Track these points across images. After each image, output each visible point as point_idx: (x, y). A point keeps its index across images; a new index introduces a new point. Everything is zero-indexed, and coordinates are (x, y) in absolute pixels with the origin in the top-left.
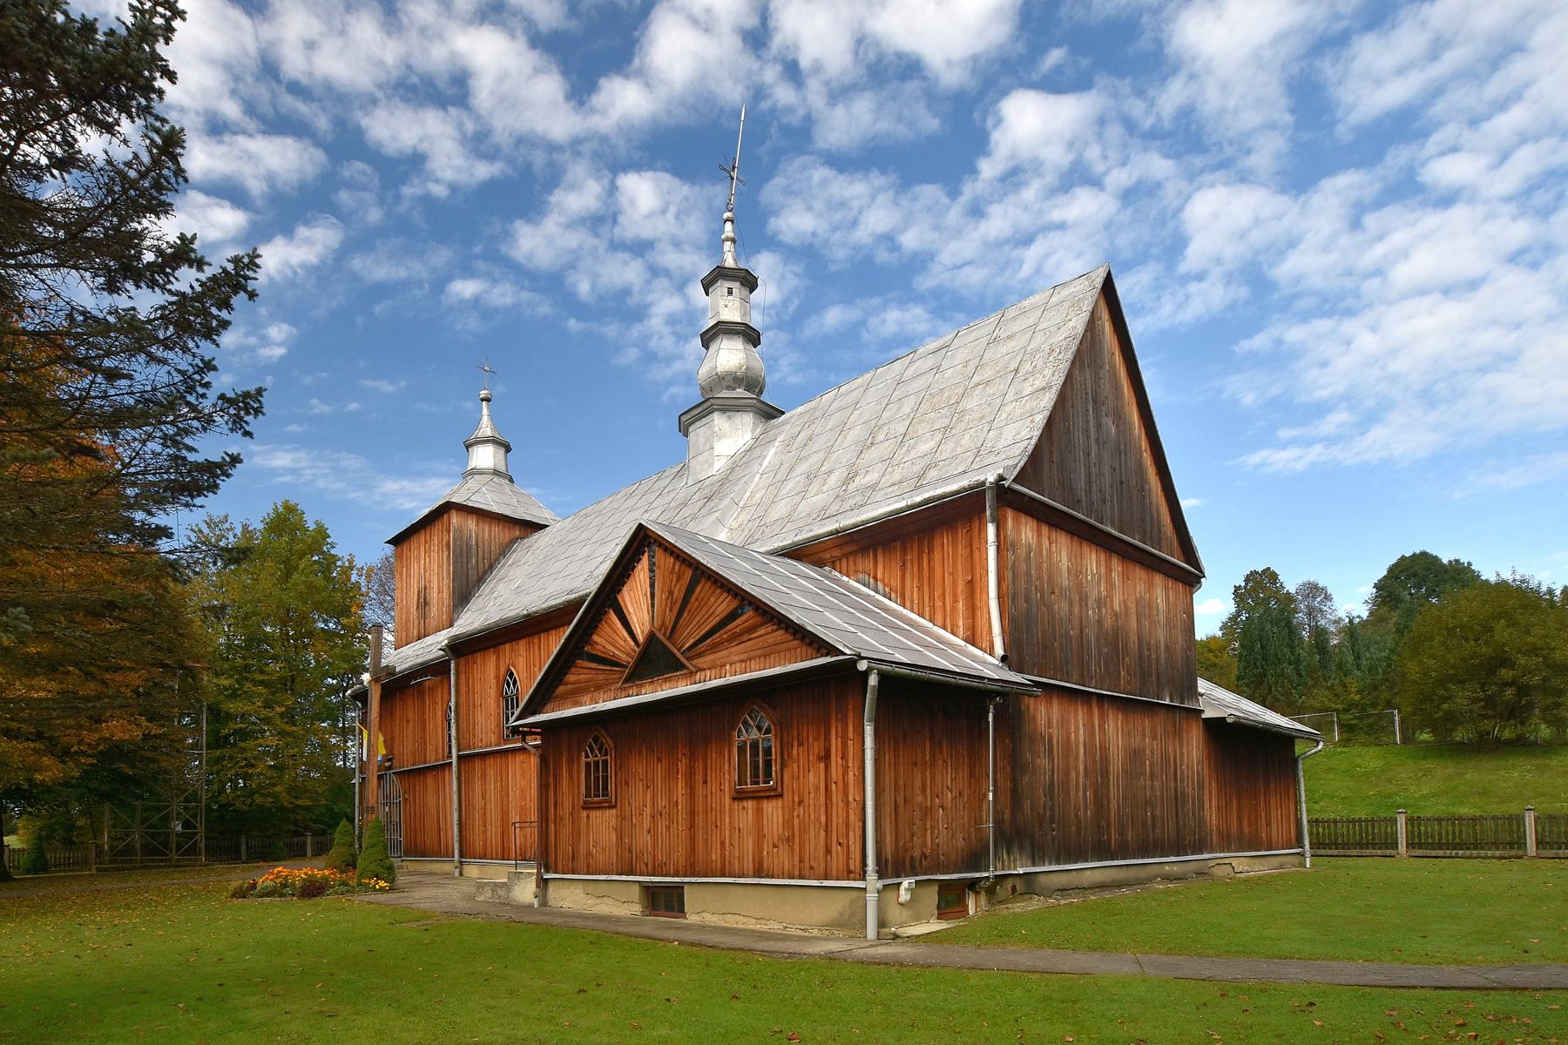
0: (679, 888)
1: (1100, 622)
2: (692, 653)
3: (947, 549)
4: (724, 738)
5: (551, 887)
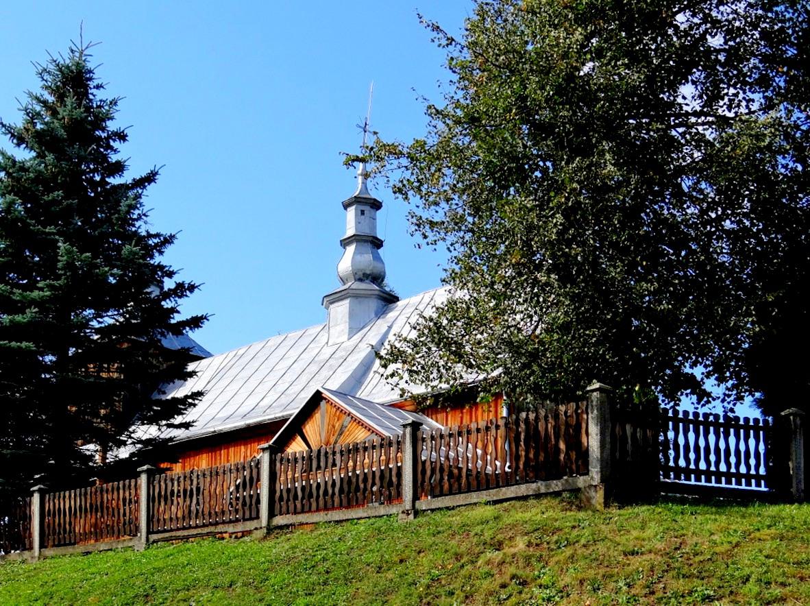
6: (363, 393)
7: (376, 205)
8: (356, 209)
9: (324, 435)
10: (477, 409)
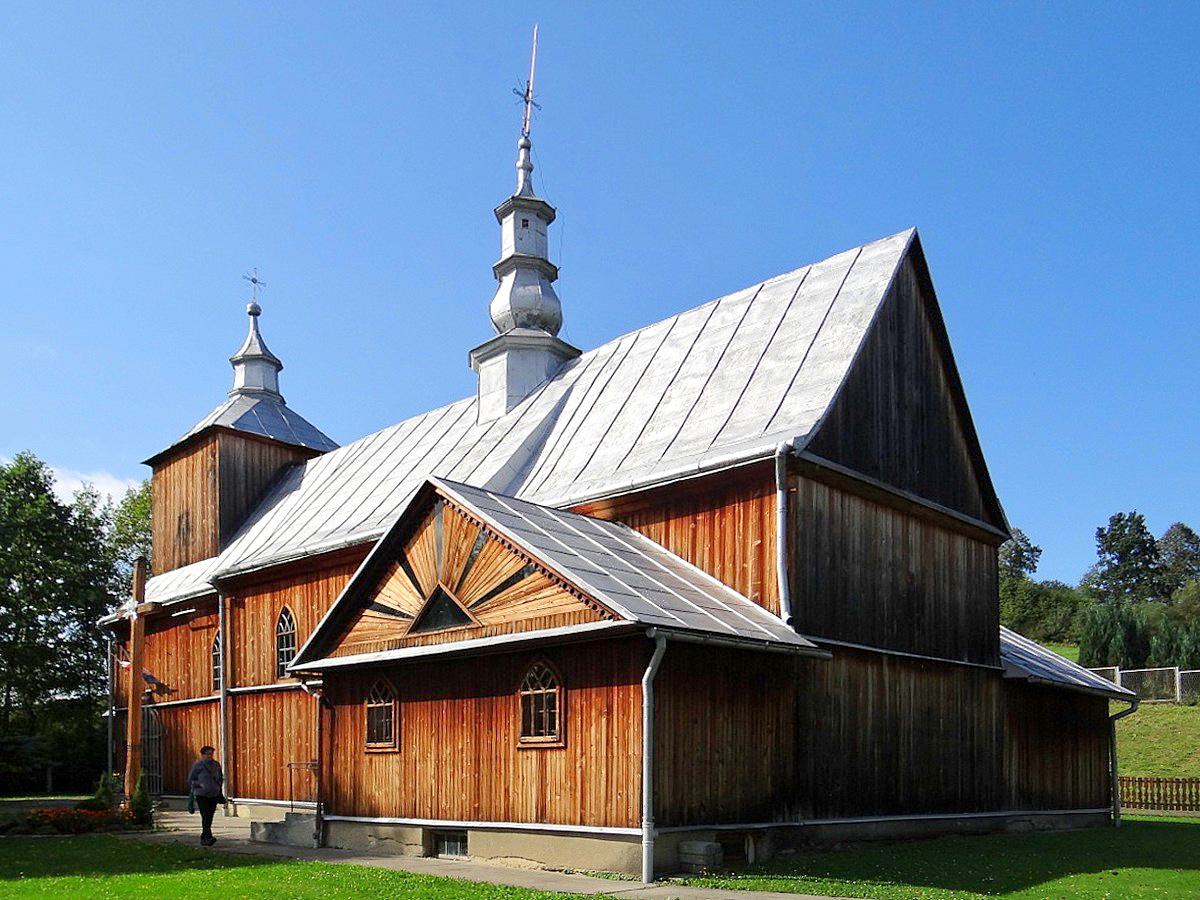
0: (464, 830)
1: (894, 586)
2: (477, 609)
3: (737, 520)
4: (510, 691)
5: (332, 828)
6: (526, 493)
7: (546, 214)
8: (515, 218)
9: (441, 567)
10: (722, 514)
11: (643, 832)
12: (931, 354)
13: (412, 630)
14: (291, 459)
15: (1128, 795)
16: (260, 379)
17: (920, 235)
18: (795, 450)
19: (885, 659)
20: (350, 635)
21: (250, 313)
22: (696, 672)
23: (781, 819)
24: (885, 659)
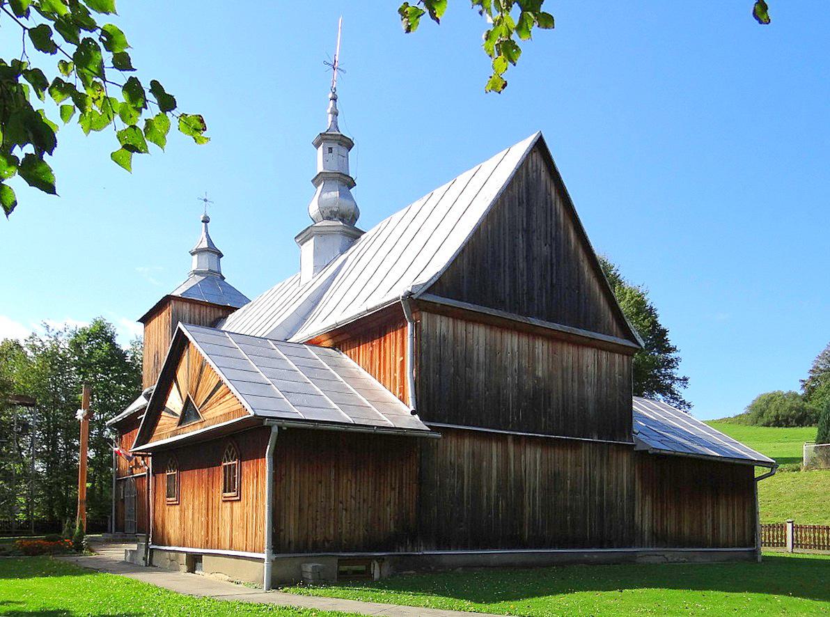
1: (519, 387)
5: (155, 553)
7: (348, 144)
11: (264, 556)
12: (562, 219)
13: (180, 424)
14: (221, 314)
15: (806, 539)
16: (205, 263)
17: (544, 136)
18: (413, 294)
19: (510, 439)
20: (158, 428)
21: (203, 221)
22: (306, 450)
23: (404, 550)
24: (510, 439)
